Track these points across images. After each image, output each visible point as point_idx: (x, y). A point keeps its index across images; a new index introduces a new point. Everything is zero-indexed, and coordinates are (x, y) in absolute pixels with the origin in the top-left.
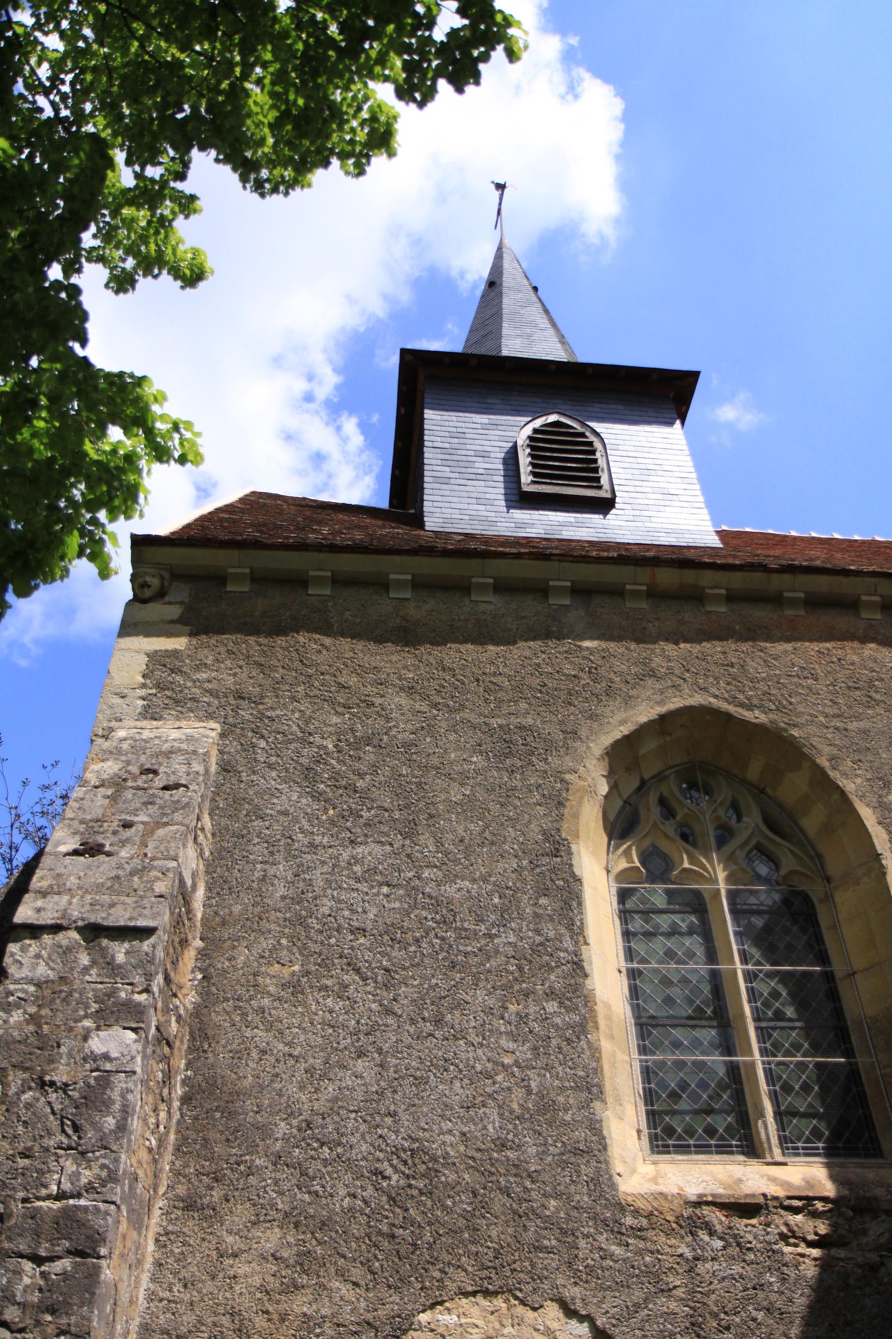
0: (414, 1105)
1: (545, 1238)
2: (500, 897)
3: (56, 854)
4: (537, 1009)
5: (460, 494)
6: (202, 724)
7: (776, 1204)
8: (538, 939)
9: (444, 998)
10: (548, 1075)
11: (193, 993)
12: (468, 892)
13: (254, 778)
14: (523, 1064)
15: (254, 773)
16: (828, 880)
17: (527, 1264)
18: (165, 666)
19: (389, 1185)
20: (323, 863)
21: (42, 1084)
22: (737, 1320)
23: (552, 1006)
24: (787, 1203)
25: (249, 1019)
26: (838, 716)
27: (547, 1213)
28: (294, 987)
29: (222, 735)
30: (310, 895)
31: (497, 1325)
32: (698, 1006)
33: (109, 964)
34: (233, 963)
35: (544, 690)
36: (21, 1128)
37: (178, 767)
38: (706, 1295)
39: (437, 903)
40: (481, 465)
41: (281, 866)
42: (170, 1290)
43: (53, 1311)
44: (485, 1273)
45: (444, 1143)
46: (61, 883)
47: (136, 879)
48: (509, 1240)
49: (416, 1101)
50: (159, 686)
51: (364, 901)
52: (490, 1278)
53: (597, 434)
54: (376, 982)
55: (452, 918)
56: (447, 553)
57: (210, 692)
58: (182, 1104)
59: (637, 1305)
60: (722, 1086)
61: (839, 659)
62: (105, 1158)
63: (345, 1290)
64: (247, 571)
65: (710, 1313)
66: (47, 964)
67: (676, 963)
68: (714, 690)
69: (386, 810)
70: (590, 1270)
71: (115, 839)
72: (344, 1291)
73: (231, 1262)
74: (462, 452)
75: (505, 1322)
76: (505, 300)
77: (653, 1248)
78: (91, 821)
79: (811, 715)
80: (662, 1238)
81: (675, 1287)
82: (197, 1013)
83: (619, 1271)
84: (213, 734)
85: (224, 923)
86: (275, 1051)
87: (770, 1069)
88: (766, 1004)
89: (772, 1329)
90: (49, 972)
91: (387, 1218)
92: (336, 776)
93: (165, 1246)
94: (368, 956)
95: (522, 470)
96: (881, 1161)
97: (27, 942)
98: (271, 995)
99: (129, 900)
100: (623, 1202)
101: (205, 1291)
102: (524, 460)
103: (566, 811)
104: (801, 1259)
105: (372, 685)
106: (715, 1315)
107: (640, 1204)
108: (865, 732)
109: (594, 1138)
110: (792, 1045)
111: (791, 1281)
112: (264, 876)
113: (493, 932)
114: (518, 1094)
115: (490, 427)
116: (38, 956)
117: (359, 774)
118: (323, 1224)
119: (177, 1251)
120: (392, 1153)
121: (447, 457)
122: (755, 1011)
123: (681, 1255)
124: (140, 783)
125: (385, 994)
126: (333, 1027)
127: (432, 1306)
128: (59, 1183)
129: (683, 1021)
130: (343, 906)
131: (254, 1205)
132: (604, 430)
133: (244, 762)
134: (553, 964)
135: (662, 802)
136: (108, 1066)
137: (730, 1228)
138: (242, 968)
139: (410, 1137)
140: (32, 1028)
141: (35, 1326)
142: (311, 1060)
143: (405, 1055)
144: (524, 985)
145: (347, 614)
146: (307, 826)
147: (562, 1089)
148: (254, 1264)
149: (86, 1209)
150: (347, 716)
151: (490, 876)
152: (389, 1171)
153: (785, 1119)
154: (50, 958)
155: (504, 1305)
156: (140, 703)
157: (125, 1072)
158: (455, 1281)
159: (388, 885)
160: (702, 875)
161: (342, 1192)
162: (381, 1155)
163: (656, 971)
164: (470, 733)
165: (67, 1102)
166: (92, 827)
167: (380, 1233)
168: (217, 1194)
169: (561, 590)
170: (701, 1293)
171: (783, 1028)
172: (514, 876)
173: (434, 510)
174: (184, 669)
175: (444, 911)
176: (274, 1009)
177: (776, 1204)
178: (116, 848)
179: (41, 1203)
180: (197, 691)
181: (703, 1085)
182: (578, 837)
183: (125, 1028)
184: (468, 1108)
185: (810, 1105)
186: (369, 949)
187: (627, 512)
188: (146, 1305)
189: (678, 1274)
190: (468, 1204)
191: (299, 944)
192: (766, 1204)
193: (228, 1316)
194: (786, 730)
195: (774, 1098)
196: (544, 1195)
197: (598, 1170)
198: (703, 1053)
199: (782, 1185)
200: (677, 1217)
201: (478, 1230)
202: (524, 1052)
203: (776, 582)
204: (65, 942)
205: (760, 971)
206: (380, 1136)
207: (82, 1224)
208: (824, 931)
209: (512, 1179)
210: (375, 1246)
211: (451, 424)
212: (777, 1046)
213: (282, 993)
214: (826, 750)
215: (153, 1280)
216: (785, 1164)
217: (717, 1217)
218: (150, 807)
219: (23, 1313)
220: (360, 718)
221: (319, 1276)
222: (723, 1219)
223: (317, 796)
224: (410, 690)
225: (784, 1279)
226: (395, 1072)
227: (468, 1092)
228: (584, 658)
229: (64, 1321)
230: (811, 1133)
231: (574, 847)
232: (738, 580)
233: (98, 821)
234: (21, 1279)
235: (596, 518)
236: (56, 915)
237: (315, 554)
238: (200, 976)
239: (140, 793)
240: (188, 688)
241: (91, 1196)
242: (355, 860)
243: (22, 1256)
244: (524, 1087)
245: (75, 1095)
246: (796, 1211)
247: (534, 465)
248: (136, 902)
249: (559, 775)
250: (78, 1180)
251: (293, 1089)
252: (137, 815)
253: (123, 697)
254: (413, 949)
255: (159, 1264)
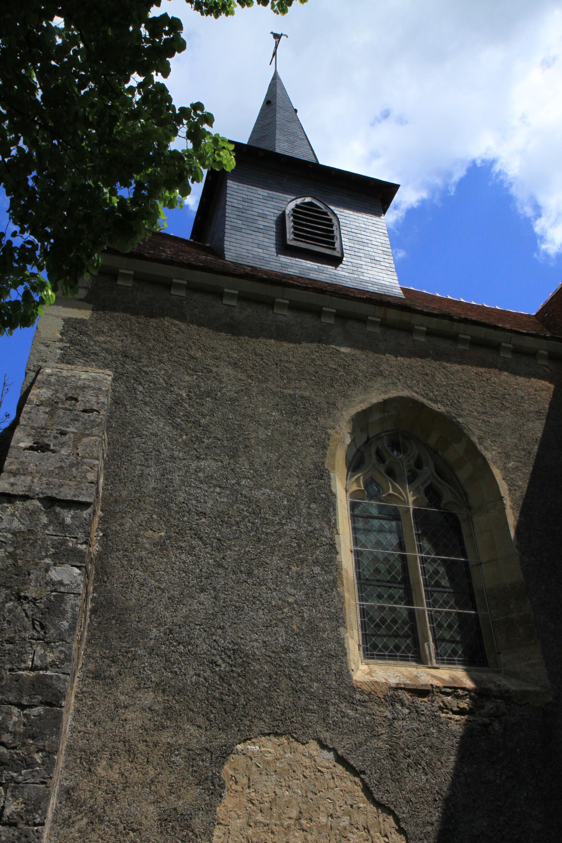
0: (235, 623)
1: (310, 704)
2: (288, 501)
3: (19, 448)
4: (309, 570)
5: (248, 240)
6: (101, 371)
7: (438, 690)
8: (310, 528)
9: (254, 559)
10: (314, 610)
11: (97, 544)
12: (269, 496)
13: (136, 410)
14: (300, 603)
15: (135, 406)
16: (470, 508)
17: (300, 719)
18: (76, 329)
19: (220, 670)
20: (180, 469)
21: (19, 598)
22: (414, 752)
23: (317, 570)
24: (443, 690)
25: (133, 563)
26: (485, 413)
27: (312, 690)
28: (161, 545)
29: (114, 380)
30: (171, 489)
31: (282, 752)
32: (393, 576)
33: (60, 524)
34: (123, 527)
35: (316, 375)
36: (6, 625)
37: (90, 397)
38: (398, 738)
39: (249, 501)
40: (261, 223)
41: (152, 469)
42: (85, 726)
43: (33, 738)
44: (276, 723)
45: (253, 647)
46: (25, 468)
47: (74, 469)
48: (290, 705)
49: (236, 621)
50: (71, 342)
51: (205, 496)
52: (278, 726)
53: (335, 215)
54: (212, 546)
55: (258, 511)
56: (262, 280)
57: (107, 350)
58: (91, 614)
59: (361, 744)
60: (404, 623)
61: (487, 379)
62: (62, 646)
63: (193, 729)
64: (132, 273)
65: (400, 748)
66: (19, 521)
67: (382, 549)
68: (416, 389)
69: (219, 440)
70: (335, 723)
71: (55, 442)
72: (192, 731)
73: (123, 711)
74: (250, 213)
75: (286, 751)
76: (278, 115)
77: (371, 712)
78: (39, 428)
79: (470, 411)
80: (376, 707)
81: (382, 734)
82: (100, 556)
83: (351, 724)
84: (110, 378)
85: (116, 501)
86: (149, 585)
87: (431, 615)
88: (431, 577)
89: (432, 757)
90: (21, 526)
91: (218, 689)
92: (188, 415)
93: (81, 700)
94: (207, 530)
95: (287, 230)
96: (487, 669)
97: (6, 505)
98: (147, 550)
99: (71, 483)
100: (355, 686)
101: (107, 728)
102: (289, 224)
103: (328, 452)
104: (450, 721)
105: (211, 359)
106: (402, 749)
107: (365, 687)
108: (498, 424)
109: (339, 649)
110: (444, 601)
111: (444, 732)
112: (142, 474)
113: (284, 522)
114: (297, 619)
115: (268, 199)
116: (13, 515)
117: (202, 415)
118: (180, 691)
119: (89, 703)
120: (222, 651)
121: (241, 214)
122: (425, 580)
123: (386, 717)
124: (67, 406)
125: (217, 554)
126: (185, 572)
127: (245, 741)
128: (33, 661)
129: (385, 584)
130: (192, 497)
131: (137, 678)
132: (338, 213)
133: (128, 399)
134: (318, 544)
135: (378, 452)
136: (62, 589)
137: (413, 703)
138: (128, 531)
139: (233, 642)
140: (11, 561)
141: (22, 746)
142: (172, 592)
143: (230, 592)
144: (301, 556)
145: (196, 311)
146: (169, 445)
147: (322, 619)
148: (137, 713)
149: (51, 677)
150: (195, 377)
151: (282, 487)
152: (220, 662)
153: (438, 643)
154: (21, 517)
155: (285, 741)
156: (59, 351)
157: (74, 594)
158: (258, 727)
159: (220, 487)
160: (399, 498)
161: (192, 673)
162: (215, 652)
163: (371, 552)
164: (271, 397)
165: (36, 610)
166: (40, 432)
167: (214, 698)
168: (114, 670)
169: (329, 314)
170: (396, 737)
171: (439, 592)
172: (296, 489)
173: (231, 247)
174: (89, 332)
175: (254, 506)
176: (149, 558)
177: (438, 690)
178: (57, 448)
179: (22, 672)
180: (98, 349)
181: (394, 621)
182: (334, 469)
183: (72, 566)
184: (267, 627)
185: (452, 636)
186: (208, 526)
187: (349, 267)
188: (70, 734)
189: (384, 727)
190: (267, 683)
191: (164, 519)
192: (432, 690)
193: (122, 743)
194: (455, 418)
195: (433, 629)
196: (311, 680)
197: (341, 667)
198: (395, 603)
199: (439, 680)
200: (385, 696)
201: (272, 698)
202: (300, 595)
203: (457, 328)
204: (31, 507)
205: (429, 558)
206: (215, 641)
207: (49, 686)
208: (465, 538)
209: (292, 670)
210: (211, 705)
211: (244, 192)
212: (435, 602)
213: (154, 549)
214: (477, 432)
215: (74, 719)
216: (438, 668)
217: (406, 697)
218: (76, 422)
219: (14, 738)
220: (203, 379)
221: (177, 722)
222: (409, 697)
223: (176, 426)
224: (235, 365)
225: (440, 731)
226: (224, 603)
227: (267, 617)
228: (341, 358)
229: (41, 743)
230: (451, 652)
231: (332, 475)
232: (434, 323)
233: (43, 428)
234: (12, 718)
235: (330, 269)
236: (24, 489)
237: (178, 268)
238: (101, 534)
239: (68, 412)
240: (92, 346)
241: (54, 670)
242: (198, 470)
243: (11, 704)
244: (300, 616)
245: (42, 606)
246: (448, 694)
247: (295, 229)
248: (77, 485)
249: (324, 429)
250: (46, 659)
251: (161, 609)
252: (68, 427)
253: (47, 346)
254: (234, 528)
255: (78, 711)
